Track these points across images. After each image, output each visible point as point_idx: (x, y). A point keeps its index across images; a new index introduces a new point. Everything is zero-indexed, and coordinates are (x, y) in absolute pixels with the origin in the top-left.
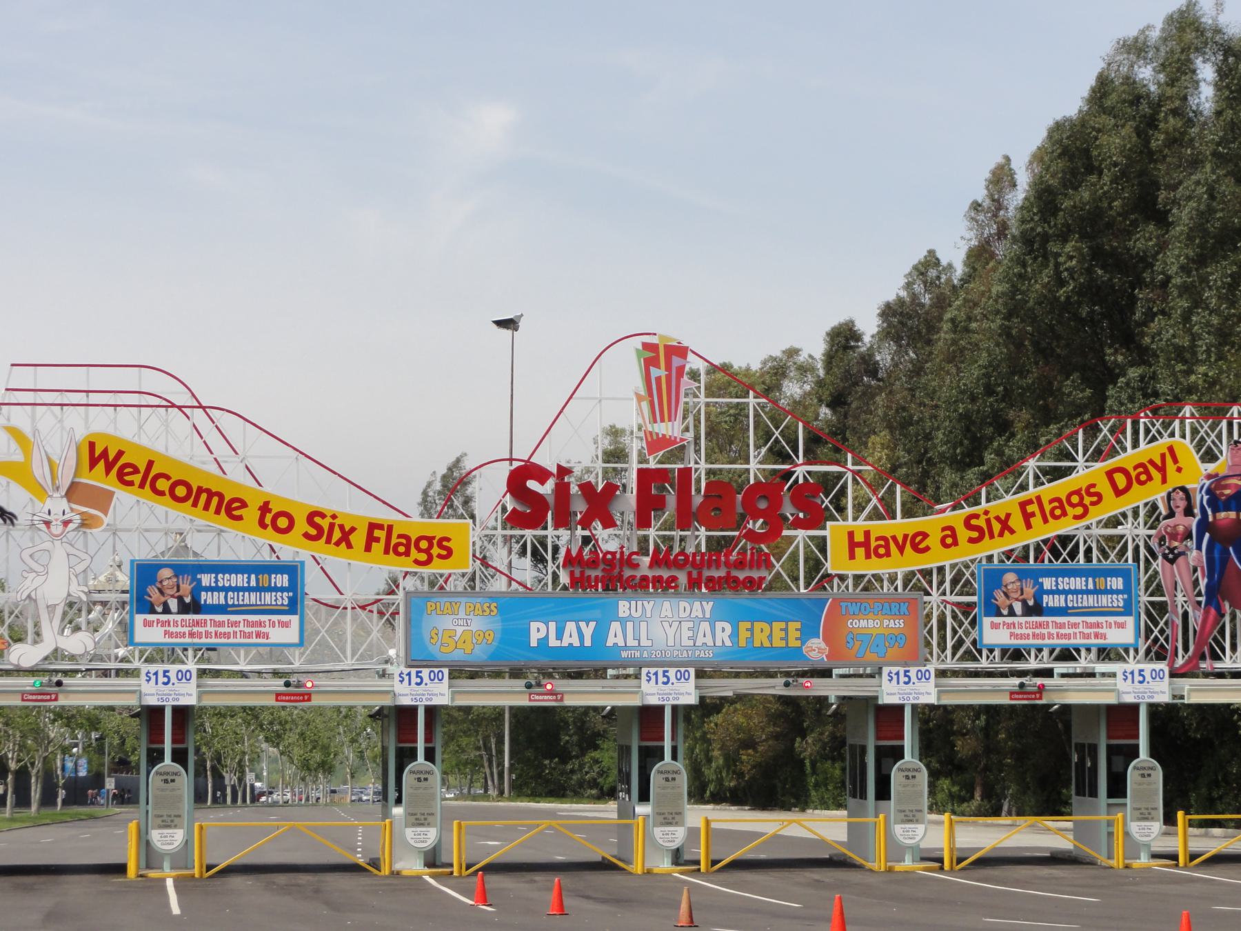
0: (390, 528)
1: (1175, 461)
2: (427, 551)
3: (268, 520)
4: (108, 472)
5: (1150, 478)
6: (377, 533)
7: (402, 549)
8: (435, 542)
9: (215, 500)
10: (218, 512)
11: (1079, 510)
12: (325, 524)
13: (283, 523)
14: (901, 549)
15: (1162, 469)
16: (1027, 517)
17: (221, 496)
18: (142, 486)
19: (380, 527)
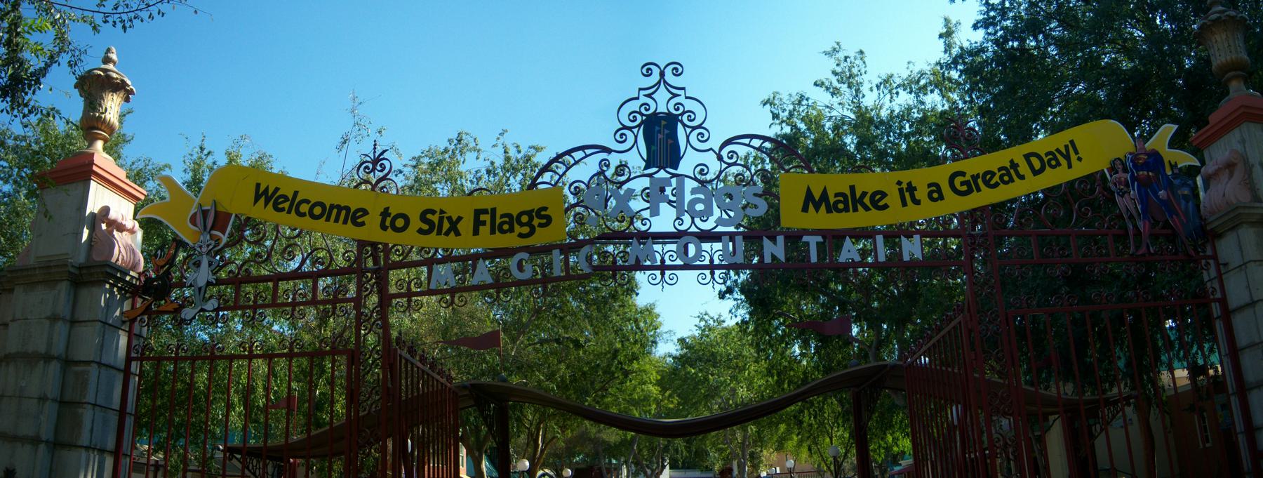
0: (494, 210)
1: (1076, 152)
2: (529, 224)
3: (388, 223)
4: (266, 204)
5: (1059, 164)
6: (483, 217)
7: (506, 227)
8: (980, 181)
9: (344, 212)
10: (345, 222)
11: (526, 230)
12: (435, 218)
13: (400, 223)
14: (824, 194)
15: (1067, 157)
16: (478, 224)
17: (348, 209)
18: (289, 212)
19: (485, 211)
